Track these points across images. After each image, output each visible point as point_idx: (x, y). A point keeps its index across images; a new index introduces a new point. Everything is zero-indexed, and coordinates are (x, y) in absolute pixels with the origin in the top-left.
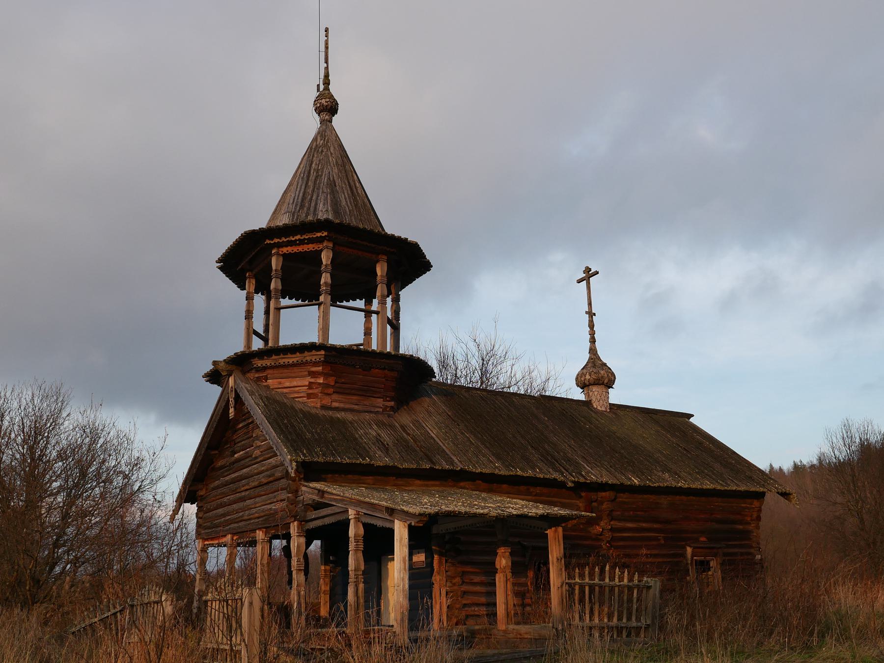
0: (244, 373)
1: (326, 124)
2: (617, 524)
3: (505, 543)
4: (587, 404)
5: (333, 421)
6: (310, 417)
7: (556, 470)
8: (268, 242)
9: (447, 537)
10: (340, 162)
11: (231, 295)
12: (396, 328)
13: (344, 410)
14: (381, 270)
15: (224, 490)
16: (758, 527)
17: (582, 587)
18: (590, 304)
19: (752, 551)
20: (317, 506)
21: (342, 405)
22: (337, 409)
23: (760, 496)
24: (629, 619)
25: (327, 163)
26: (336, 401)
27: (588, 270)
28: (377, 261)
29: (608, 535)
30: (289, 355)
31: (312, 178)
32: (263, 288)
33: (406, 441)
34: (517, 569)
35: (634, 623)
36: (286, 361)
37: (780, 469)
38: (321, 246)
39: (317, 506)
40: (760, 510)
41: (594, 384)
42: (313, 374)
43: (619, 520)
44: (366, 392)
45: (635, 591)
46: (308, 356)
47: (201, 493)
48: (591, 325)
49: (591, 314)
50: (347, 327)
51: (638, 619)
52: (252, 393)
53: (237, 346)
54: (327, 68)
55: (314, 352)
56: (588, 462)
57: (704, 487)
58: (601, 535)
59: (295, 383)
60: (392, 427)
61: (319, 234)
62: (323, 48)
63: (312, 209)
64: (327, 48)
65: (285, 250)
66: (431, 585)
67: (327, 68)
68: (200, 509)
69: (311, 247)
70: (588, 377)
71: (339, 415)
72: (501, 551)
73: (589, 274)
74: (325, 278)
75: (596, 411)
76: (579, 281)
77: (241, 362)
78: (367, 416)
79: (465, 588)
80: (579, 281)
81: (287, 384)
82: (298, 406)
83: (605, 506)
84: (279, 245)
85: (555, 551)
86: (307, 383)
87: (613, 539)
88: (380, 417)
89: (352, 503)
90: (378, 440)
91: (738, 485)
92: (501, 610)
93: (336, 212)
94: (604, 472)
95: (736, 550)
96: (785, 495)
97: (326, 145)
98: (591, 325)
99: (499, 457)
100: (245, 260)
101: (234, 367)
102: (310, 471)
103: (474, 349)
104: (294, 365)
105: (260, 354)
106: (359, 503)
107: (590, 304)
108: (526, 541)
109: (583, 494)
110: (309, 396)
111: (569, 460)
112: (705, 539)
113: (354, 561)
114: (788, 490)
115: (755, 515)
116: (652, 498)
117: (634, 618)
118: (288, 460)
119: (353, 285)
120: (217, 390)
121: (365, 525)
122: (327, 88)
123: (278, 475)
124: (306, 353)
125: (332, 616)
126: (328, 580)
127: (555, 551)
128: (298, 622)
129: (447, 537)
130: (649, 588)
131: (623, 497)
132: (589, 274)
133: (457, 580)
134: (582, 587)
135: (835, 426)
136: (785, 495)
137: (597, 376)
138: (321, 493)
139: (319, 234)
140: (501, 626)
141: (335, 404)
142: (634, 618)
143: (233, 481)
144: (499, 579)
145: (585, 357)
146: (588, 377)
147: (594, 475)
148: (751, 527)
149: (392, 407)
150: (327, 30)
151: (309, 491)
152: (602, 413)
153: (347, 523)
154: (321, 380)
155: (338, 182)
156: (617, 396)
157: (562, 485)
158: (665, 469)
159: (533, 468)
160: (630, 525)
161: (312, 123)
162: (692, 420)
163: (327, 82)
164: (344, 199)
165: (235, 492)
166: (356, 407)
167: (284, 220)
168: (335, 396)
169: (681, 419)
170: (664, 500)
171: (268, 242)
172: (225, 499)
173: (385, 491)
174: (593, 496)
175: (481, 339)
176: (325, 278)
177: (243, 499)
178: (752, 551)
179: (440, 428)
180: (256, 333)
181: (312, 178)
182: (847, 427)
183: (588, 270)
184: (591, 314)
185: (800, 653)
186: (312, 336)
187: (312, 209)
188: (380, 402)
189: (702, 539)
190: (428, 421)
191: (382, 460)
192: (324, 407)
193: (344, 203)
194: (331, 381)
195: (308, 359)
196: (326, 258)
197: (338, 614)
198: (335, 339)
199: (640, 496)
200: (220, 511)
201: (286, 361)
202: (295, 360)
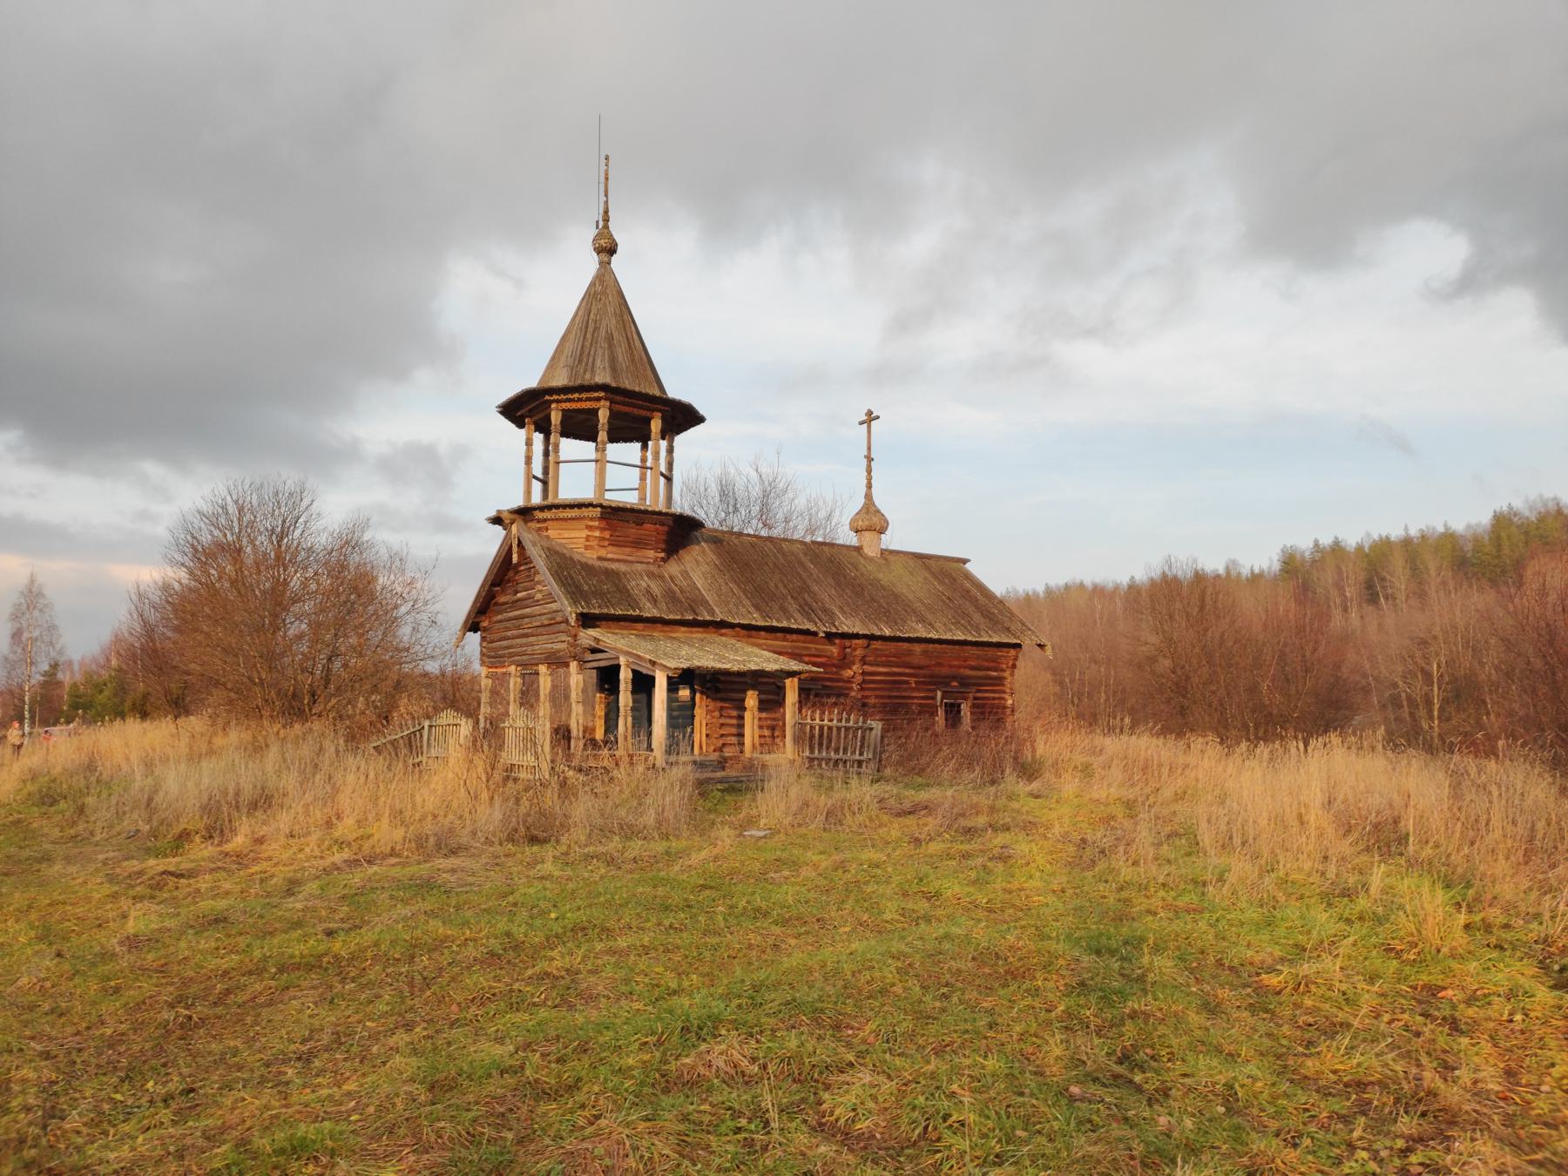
0: (526, 522)
1: (605, 266)
2: (868, 668)
3: (753, 687)
4: (858, 549)
5: (609, 573)
6: (588, 569)
7: (810, 620)
11: (513, 437)
12: (669, 479)
15: (508, 624)
16: (1012, 674)
17: (821, 728)
18: (869, 449)
20: (594, 651)
23: (1018, 646)
24: (853, 753)
27: (870, 413)
29: (859, 678)
31: (590, 329)
32: (544, 427)
33: (673, 592)
34: (764, 706)
35: (857, 757)
39: (594, 651)
40: (1016, 658)
42: (589, 528)
44: (638, 544)
46: (585, 512)
47: (484, 624)
48: (869, 471)
49: (870, 459)
51: (861, 754)
52: (534, 544)
53: (519, 502)
56: (844, 612)
60: (661, 577)
62: (602, 180)
66: (693, 716)
68: (483, 639)
69: (588, 405)
71: (614, 566)
72: (750, 693)
73: (870, 418)
75: (866, 558)
76: (861, 423)
77: (524, 513)
78: (639, 567)
79: (722, 721)
80: (861, 423)
82: (576, 557)
83: (858, 652)
85: (791, 697)
87: (864, 681)
88: (651, 568)
89: (625, 648)
90: (648, 592)
92: (748, 740)
93: (614, 370)
94: (858, 623)
96: (1041, 646)
97: (604, 293)
98: (869, 471)
99: (757, 608)
100: (523, 409)
102: (587, 620)
103: (754, 475)
105: (542, 508)
106: (628, 654)
107: (869, 449)
108: (769, 687)
110: (587, 548)
111: (825, 610)
113: (625, 698)
114: (1044, 641)
118: (570, 612)
119: (630, 428)
120: (499, 531)
121: (634, 671)
122: (606, 227)
123: (559, 619)
125: (606, 743)
127: (791, 697)
128: (577, 745)
131: (876, 645)
132: (870, 418)
133: (717, 714)
134: (812, 728)
136: (1041, 646)
137: (871, 520)
138: (597, 640)
143: (516, 618)
144: (747, 715)
148: (1006, 674)
150: (607, 158)
151: (588, 636)
152: (871, 560)
153: (618, 667)
154: (597, 534)
155: (616, 335)
156: (894, 540)
157: (815, 634)
158: (922, 620)
159: (788, 619)
160: (881, 669)
161: (589, 264)
162: (968, 566)
165: (519, 628)
167: (560, 380)
168: (610, 548)
170: (918, 648)
172: (509, 633)
173: (652, 638)
174: (847, 643)
175: (763, 470)
177: (526, 636)
181: (590, 329)
183: (870, 413)
184: (870, 459)
186: (586, 493)
188: (651, 554)
190: (695, 569)
191: (650, 611)
192: (600, 558)
194: (607, 534)
197: (610, 742)
198: (613, 498)
200: (504, 643)
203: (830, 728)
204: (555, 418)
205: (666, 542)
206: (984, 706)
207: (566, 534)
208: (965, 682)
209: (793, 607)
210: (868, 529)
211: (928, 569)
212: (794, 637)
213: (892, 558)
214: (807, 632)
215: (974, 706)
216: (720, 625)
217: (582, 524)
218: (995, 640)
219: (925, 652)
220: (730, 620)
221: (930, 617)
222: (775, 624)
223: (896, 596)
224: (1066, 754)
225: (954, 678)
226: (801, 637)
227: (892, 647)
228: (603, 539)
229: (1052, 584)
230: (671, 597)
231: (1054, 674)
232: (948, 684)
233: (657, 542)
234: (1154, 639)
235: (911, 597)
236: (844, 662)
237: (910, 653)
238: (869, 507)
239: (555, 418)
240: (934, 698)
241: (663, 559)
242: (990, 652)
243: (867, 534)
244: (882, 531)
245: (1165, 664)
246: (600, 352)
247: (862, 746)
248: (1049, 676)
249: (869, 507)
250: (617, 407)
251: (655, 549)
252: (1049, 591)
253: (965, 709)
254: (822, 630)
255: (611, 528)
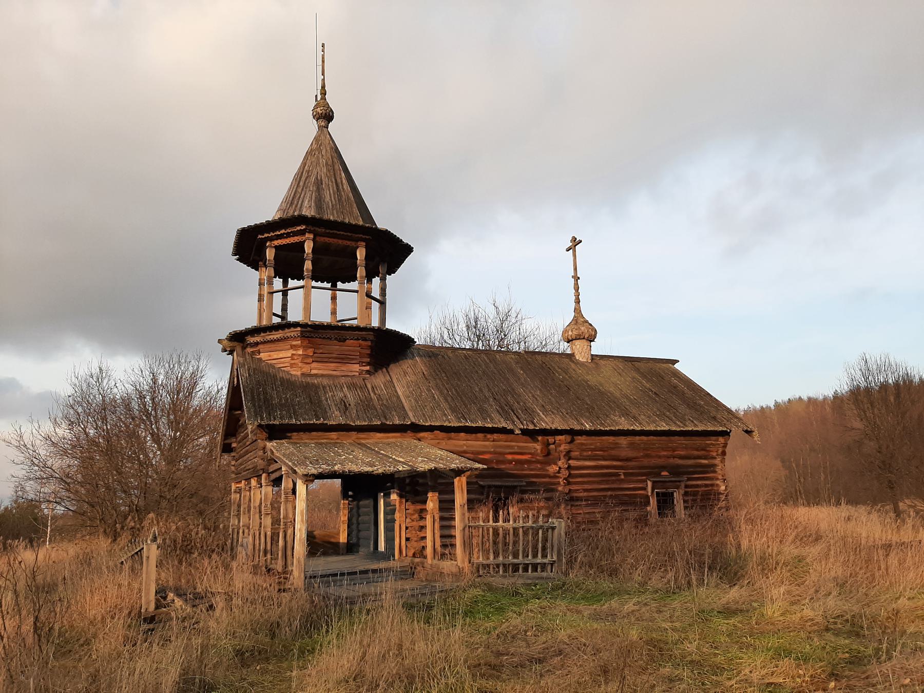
1: (323, 129)
3: (434, 490)
7: (506, 419)
8: (260, 236)
9: (408, 481)
10: (330, 163)
13: (322, 375)
14: (361, 254)
16: (723, 461)
18: (575, 269)
19: (718, 482)
21: (320, 372)
22: (316, 375)
23: (725, 434)
24: (535, 556)
25: (326, 164)
26: (315, 369)
27: (574, 239)
28: (358, 247)
29: (565, 473)
30: (274, 332)
31: (303, 178)
35: (539, 560)
36: (271, 337)
37: (800, 398)
38: (304, 238)
41: (576, 339)
43: (577, 459)
44: (343, 359)
45: (540, 532)
48: (577, 288)
49: (576, 278)
50: (343, 304)
51: (544, 556)
54: (323, 80)
55: (292, 329)
57: (659, 429)
58: (559, 472)
59: (281, 356)
61: (299, 228)
63: (299, 206)
64: (323, 61)
65: (276, 243)
67: (323, 80)
70: (570, 333)
72: (430, 495)
73: (575, 242)
74: (308, 265)
75: (577, 363)
81: (275, 357)
83: (562, 448)
84: (271, 239)
85: (460, 497)
86: (290, 355)
87: (570, 475)
91: (696, 425)
95: (699, 482)
96: (749, 432)
98: (577, 288)
99: (454, 410)
101: (235, 344)
104: (278, 340)
107: (575, 269)
109: (540, 438)
110: (292, 366)
111: (526, 410)
112: (666, 473)
115: (720, 450)
116: (611, 439)
117: (540, 555)
119: (334, 270)
122: (323, 98)
124: (287, 330)
126: (346, 512)
127: (460, 497)
129: (408, 481)
130: (553, 528)
131: (580, 440)
132: (575, 242)
135: (854, 359)
136: (749, 432)
137: (580, 330)
139: (299, 228)
140: (429, 561)
141: (314, 372)
142: (540, 555)
144: (428, 522)
145: (571, 316)
146: (570, 333)
147: (547, 421)
149: (367, 371)
150: (323, 46)
154: (300, 352)
156: (599, 347)
157: (511, 432)
158: (626, 414)
159: (484, 419)
161: (312, 127)
162: (676, 366)
163: (324, 93)
164: (328, 196)
166: (335, 373)
168: (314, 365)
169: (665, 365)
170: (623, 441)
171: (260, 236)
174: (551, 439)
176: (308, 265)
178: (718, 482)
179: (408, 387)
180: (275, 315)
181: (303, 178)
182: (887, 356)
183: (574, 239)
184: (576, 278)
185: (701, 582)
187: (299, 206)
188: (356, 367)
189: (664, 473)
190: (402, 383)
191: (337, 418)
193: (328, 199)
194: (310, 352)
195: (288, 335)
196: (308, 247)
199: (598, 438)
201: (271, 337)
202: (278, 336)
203: (506, 533)
204: (270, 254)
205: (370, 356)
206: (695, 494)
207: (275, 355)
208: (676, 471)
209: (492, 407)
210: (578, 338)
211: (638, 370)
212: (495, 436)
213: (602, 362)
214: (503, 431)
215: (686, 494)
216: (415, 428)
217: (286, 345)
218: (700, 428)
219: (631, 445)
220: (422, 423)
221: (634, 411)
222: (469, 424)
223: (602, 394)
224: (774, 548)
225: (664, 468)
226: (501, 436)
227: (597, 441)
228: (307, 356)
229: (779, 400)
230: (366, 405)
231: (783, 462)
232: (659, 475)
233: (361, 356)
234: (858, 424)
235: (617, 394)
236: (548, 456)
237: (616, 446)
238: (578, 318)
239: (270, 254)
240: (645, 489)
241: (368, 372)
242: (698, 441)
243: (577, 342)
244: (591, 339)
245: (870, 446)
246: (308, 195)
247: (544, 549)
248: (778, 463)
249: (578, 318)
250: (321, 239)
251: (361, 363)
252: (777, 405)
253: (678, 496)
254: (518, 427)
255: (315, 346)
